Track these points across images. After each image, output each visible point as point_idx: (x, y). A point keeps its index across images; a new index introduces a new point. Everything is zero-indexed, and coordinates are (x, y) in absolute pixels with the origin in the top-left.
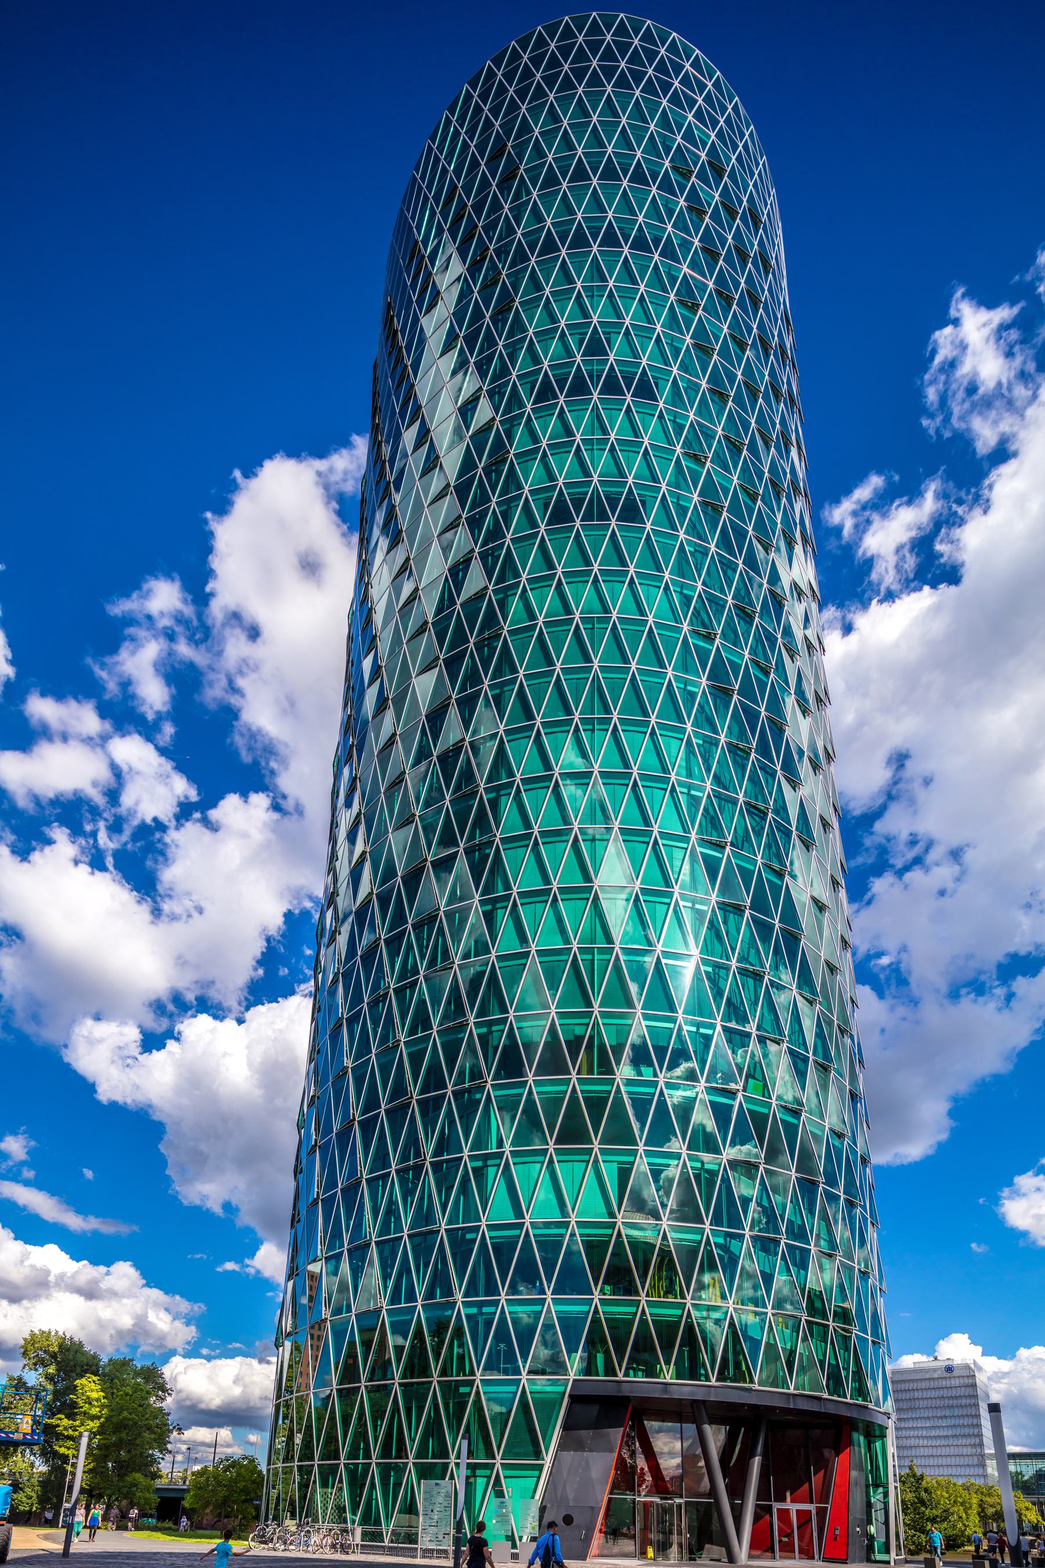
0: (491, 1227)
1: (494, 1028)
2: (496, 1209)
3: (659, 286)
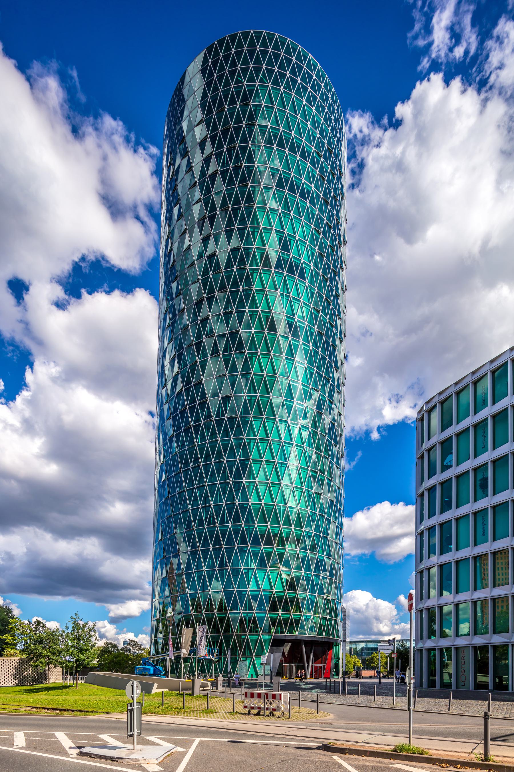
0: (250, 591)
1: (254, 313)
2: (252, 587)
3: (287, 168)
